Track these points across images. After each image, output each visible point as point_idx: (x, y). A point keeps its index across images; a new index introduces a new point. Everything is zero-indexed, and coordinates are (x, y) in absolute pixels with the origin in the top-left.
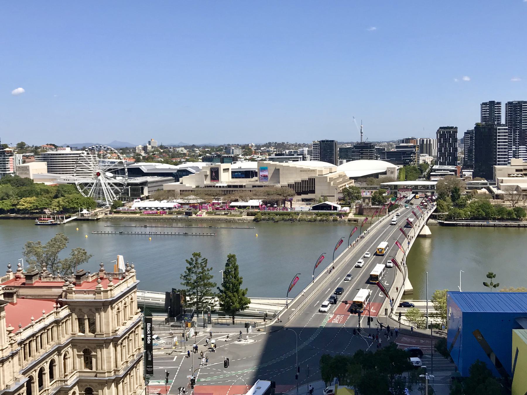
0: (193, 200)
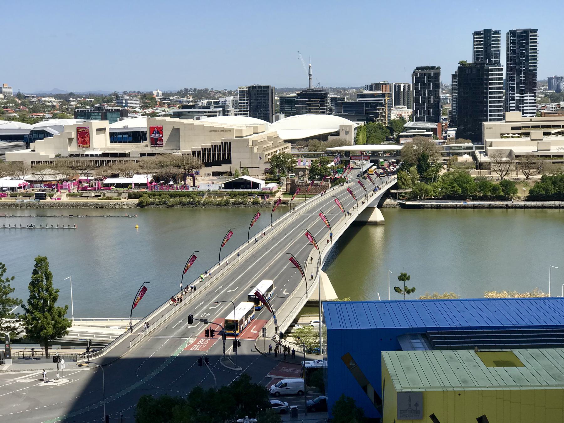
0: (49, 175)
